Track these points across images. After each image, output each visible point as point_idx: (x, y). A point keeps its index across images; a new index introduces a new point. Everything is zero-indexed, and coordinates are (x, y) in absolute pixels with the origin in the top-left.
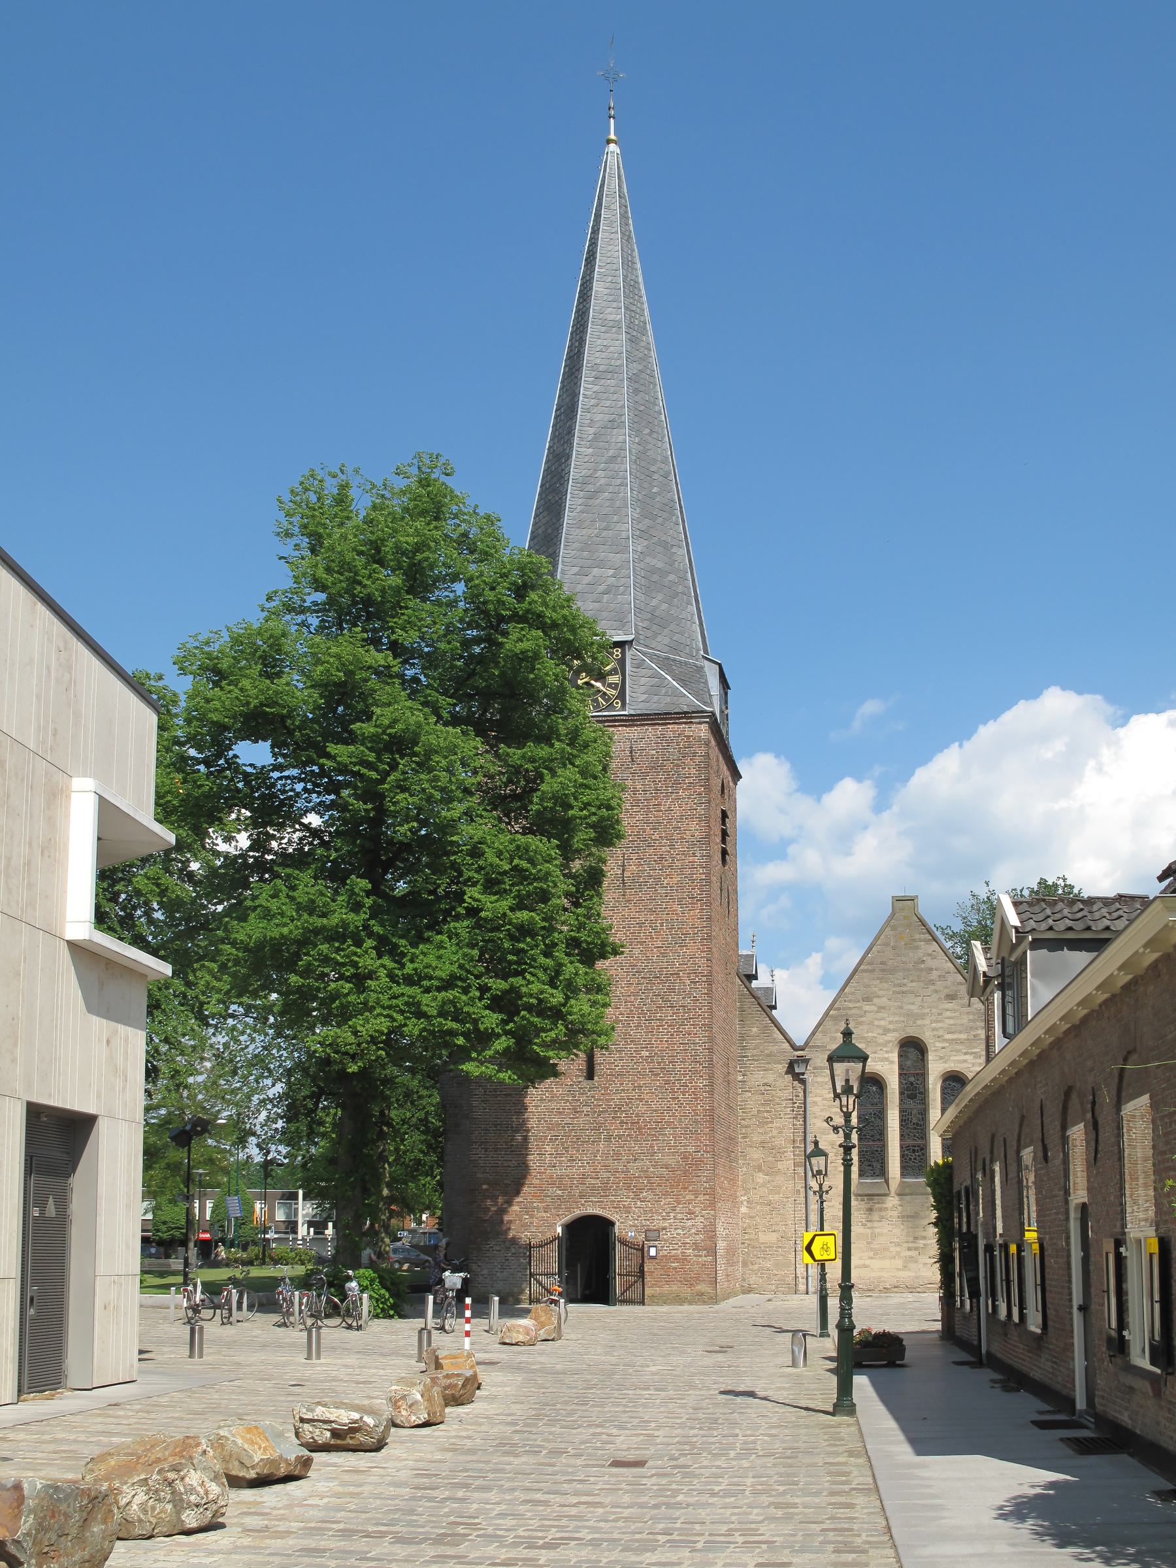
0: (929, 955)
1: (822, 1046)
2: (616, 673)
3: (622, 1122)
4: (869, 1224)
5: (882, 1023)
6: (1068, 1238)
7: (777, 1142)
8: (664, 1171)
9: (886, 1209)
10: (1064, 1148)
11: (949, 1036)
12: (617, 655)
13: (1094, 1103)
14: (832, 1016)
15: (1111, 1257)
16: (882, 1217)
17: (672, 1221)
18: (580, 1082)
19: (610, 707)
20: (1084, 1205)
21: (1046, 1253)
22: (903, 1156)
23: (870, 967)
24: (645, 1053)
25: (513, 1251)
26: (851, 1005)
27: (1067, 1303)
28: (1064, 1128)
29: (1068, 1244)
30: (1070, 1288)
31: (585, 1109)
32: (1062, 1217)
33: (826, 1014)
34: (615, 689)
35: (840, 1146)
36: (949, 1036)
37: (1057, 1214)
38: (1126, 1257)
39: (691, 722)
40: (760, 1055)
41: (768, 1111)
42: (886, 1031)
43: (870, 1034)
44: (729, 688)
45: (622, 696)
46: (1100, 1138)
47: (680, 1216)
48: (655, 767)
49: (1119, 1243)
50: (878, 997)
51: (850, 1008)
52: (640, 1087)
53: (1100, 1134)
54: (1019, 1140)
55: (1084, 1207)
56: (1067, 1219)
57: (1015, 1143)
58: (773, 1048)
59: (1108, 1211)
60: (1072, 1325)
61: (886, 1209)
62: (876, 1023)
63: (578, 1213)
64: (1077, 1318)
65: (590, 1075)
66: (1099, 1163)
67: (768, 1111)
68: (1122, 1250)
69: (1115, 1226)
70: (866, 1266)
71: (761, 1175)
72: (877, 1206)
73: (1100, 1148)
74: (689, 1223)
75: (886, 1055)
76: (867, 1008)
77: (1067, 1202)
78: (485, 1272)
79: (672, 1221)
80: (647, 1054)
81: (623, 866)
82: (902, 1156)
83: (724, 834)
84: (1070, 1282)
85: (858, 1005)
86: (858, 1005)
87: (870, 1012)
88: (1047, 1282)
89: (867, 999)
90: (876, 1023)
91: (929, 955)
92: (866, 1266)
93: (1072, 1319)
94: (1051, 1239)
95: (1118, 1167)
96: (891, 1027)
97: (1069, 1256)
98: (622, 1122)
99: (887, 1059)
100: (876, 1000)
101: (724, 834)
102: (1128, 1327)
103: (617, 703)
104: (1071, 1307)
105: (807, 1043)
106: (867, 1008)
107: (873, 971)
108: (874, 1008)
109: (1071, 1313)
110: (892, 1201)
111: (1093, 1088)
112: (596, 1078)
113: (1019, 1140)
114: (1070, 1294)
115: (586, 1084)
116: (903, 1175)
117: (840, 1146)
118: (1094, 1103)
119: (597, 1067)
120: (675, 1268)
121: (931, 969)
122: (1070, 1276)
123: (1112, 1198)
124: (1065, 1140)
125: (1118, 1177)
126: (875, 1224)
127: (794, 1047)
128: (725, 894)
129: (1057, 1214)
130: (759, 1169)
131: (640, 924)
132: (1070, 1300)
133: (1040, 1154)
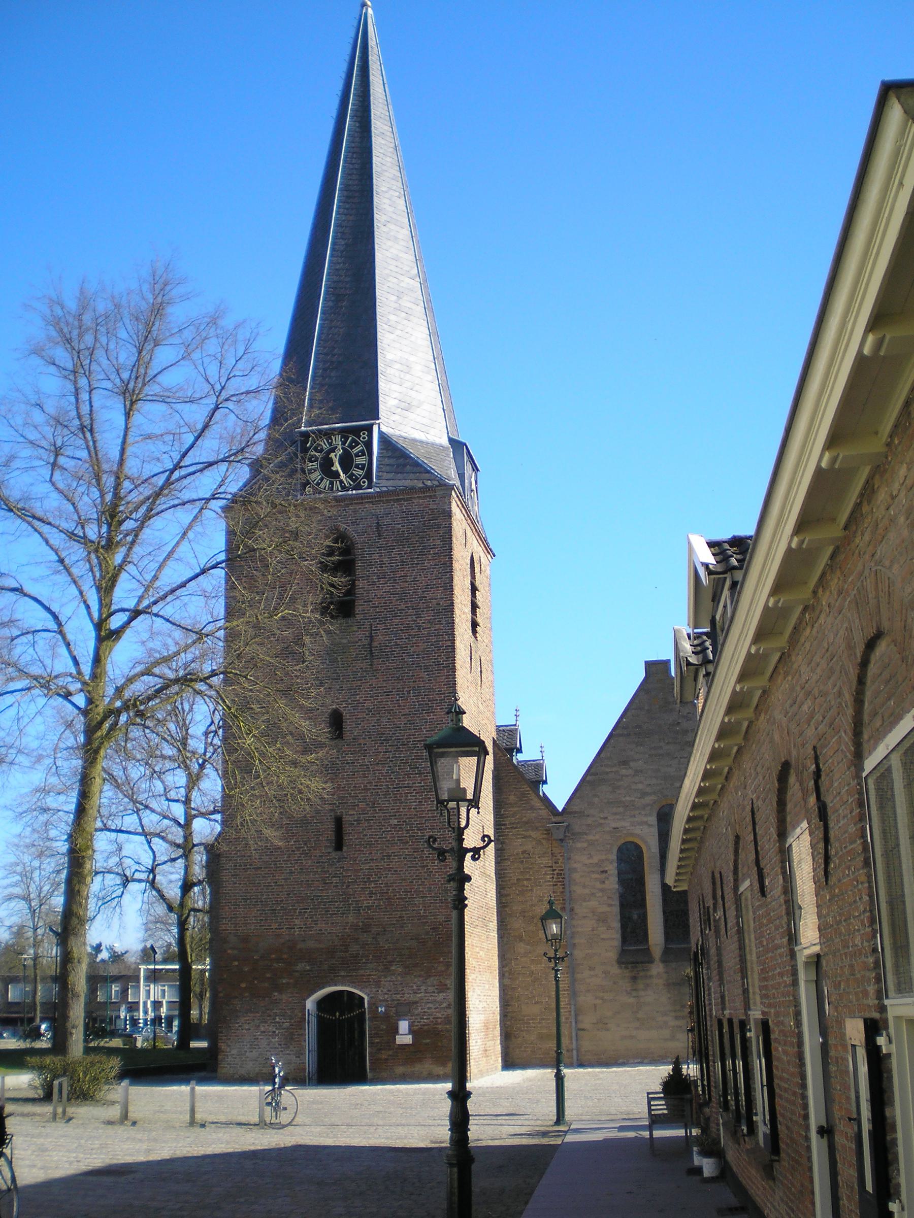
0: (684, 717)
1: (580, 812)
2: (363, 454)
3: (371, 893)
4: (634, 994)
5: (640, 786)
6: (798, 1014)
9: (651, 977)
10: (783, 868)
12: (364, 434)
13: (818, 774)
14: (589, 782)
15: (861, 1053)
16: (648, 985)
17: (422, 995)
18: (329, 853)
20: (818, 956)
21: (772, 1037)
25: (262, 1029)
26: (608, 770)
27: (801, 1121)
28: (782, 834)
29: (798, 1024)
30: (804, 1097)
31: (335, 880)
32: (788, 979)
34: (362, 469)
37: (781, 975)
38: (889, 1055)
40: (518, 823)
41: (527, 879)
42: (644, 794)
43: (628, 798)
44: (478, 470)
46: (832, 834)
47: (430, 989)
49: (873, 1028)
50: (634, 760)
51: (607, 773)
52: (389, 856)
53: (831, 824)
54: (736, 871)
55: (817, 961)
56: (795, 983)
57: (731, 878)
58: (531, 815)
59: (851, 966)
60: (810, 1159)
61: (651, 977)
62: (634, 787)
64: (817, 1145)
65: (339, 845)
66: (833, 880)
67: (527, 879)
68: (881, 1041)
69: (866, 994)
70: (632, 1037)
71: (522, 945)
72: (641, 974)
73: (832, 852)
74: (442, 996)
75: (645, 819)
76: (624, 772)
77: (793, 955)
78: (234, 1052)
79: (422, 995)
80: (395, 822)
81: (371, 637)
84: (804, 1086)
85: (614, 769)
86: (614, 769)
87: (627, 776)
88: (776, 1081)
89: (625, 763)
90: (634, 787)
91: (684, 717)
92: (632, 1037)
93: (809, 1148)
94: (777, 1014)
95: (863, 878)
96: (648, 790)
97: (800, 1044)
98: (371, 893)
99: (646, 823)
100: (632, 764)
101: (474, 607)
102: (898, 1195)
103: (364, 482)
104: (807, 1128)
106: (624, 772)
107: (628, 735)
108: (630, 772)
109: (807, 1139)
110: (657, 968)
111: (815, 748)
112: (345, 848)
113: (736, 871)
114: (805, 1106)
115: (335, 855)
118: (818, 774)
120: (427, 1044)
121: (687, 731)
122: (803, 1076)
123: (858, 941)
124: (785, 854)
125: (866, 898)
126: (642, 993)
128: (476, 664)
129: (781, 975)
131: (388, 693)
132: (806, 1117)
133: (757, 886)
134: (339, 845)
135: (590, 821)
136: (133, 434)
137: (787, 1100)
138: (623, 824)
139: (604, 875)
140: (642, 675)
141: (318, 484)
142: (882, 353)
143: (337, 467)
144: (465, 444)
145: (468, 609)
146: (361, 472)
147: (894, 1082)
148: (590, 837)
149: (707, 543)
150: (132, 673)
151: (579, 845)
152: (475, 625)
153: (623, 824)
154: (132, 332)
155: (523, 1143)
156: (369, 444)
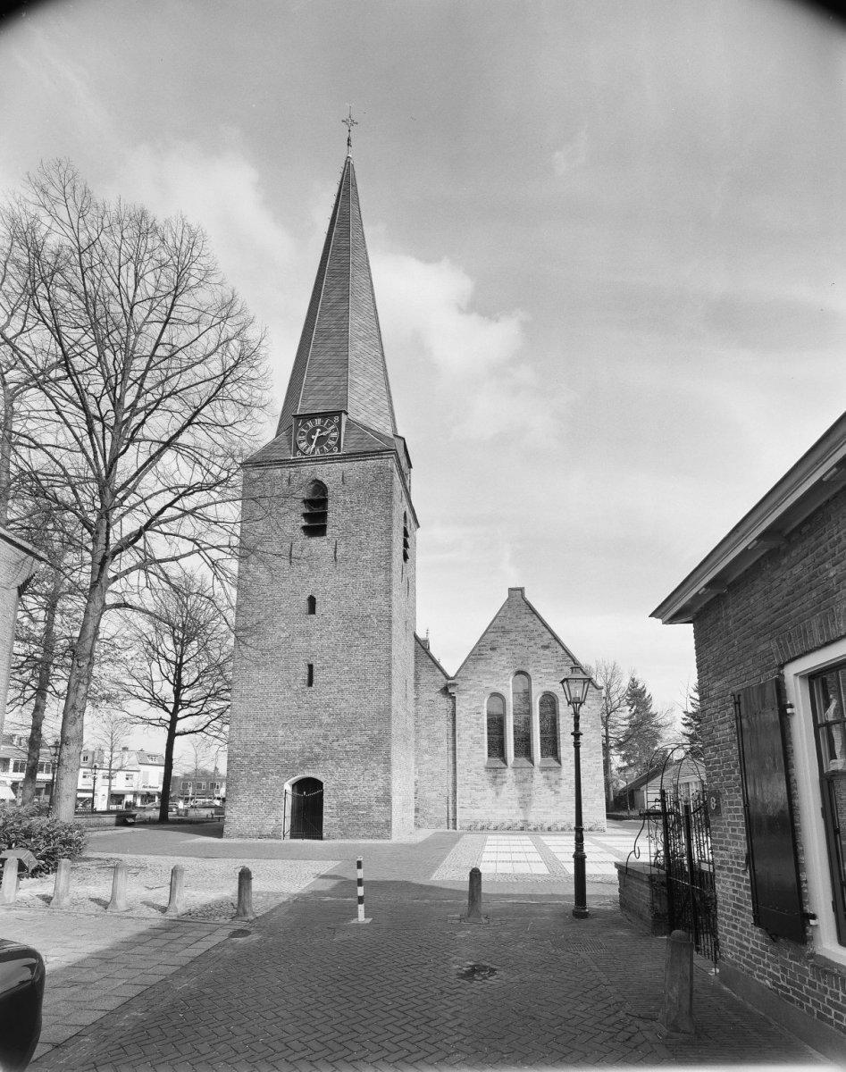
7: (438, 735)
8: (357, 748)
9: (505, 777)
11: (545, 671)
19: (331, 451)
22: (516, 745)
23: (495, 630)
24: (346, 668)
33: (468, 657)
35: (572, 734)
36: (545, 671)
39: (382, 458)
45: (338, 444)
48: (359, 486)
61: (505, 777)
63: (300, 776)
65: (310, 683)
82: (515, 745)
83: (406, 545)
101: (406, 545)
105: (456, 675)
110: (509, 772)
115: (307, 689)
116: (515, 755)
117: (572, 734)
119: (315, 678)
127: (448, 678)
130: (426, 752)
134: (310, 683)
135: (471, 682)
136: (180, 418)
137: (726, 917)
138: (491, 685)
139: (479, 715)
140: (506, 596)
141: (305, 450)
142: (824, 479)
143: (315, 437)
144: (404, 439)
145: (402, 536)
146: (334, 443)
147: (513, 740)
148: (472, 693)
149: (655, 614)
150: (111, 531)
151: (464, 697)
152: (406, 557)
153: (491, 685)
154: (73, 238)
155: (290, 815)
156: (339, 425)
